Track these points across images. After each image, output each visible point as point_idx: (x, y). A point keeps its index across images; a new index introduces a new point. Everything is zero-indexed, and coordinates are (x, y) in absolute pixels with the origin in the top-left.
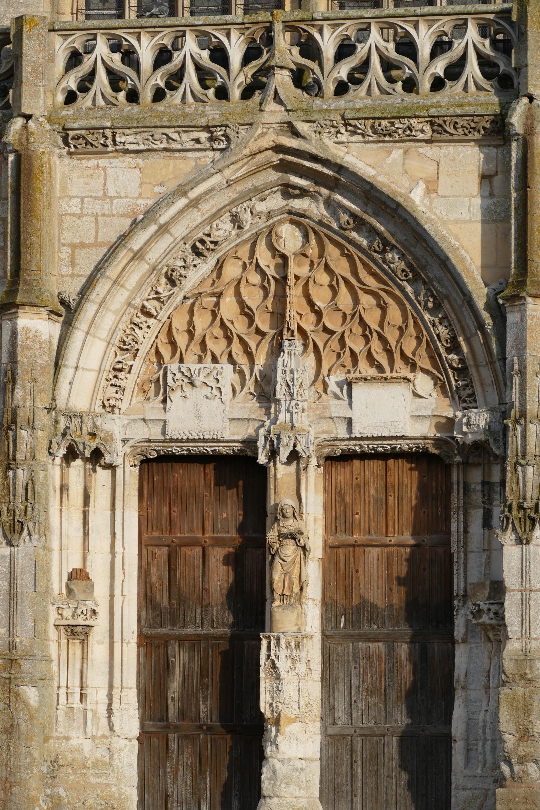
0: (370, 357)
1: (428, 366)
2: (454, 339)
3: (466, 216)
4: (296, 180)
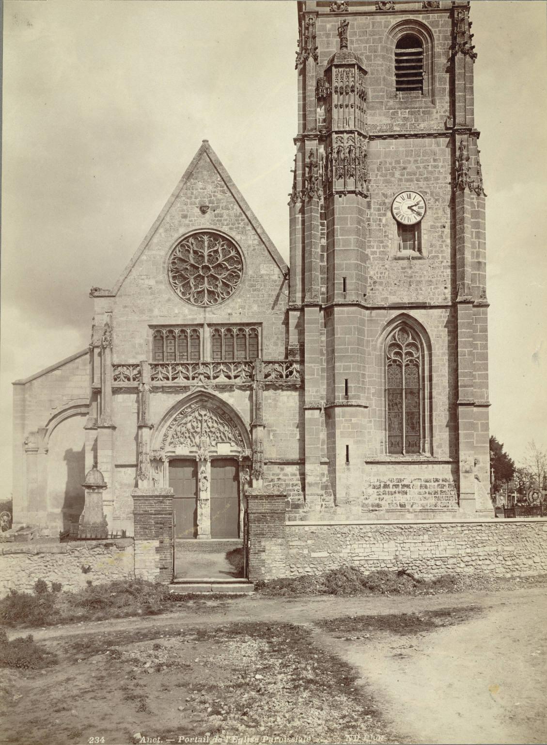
0: (221, 437)
1: (234, 439)
2: (240, 434)
3: (295, 482)
4: (204, 398)
